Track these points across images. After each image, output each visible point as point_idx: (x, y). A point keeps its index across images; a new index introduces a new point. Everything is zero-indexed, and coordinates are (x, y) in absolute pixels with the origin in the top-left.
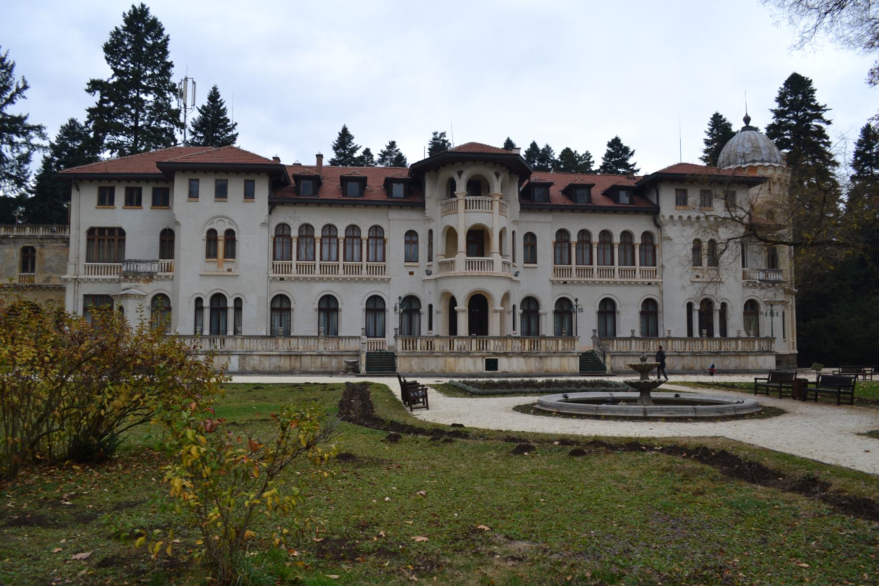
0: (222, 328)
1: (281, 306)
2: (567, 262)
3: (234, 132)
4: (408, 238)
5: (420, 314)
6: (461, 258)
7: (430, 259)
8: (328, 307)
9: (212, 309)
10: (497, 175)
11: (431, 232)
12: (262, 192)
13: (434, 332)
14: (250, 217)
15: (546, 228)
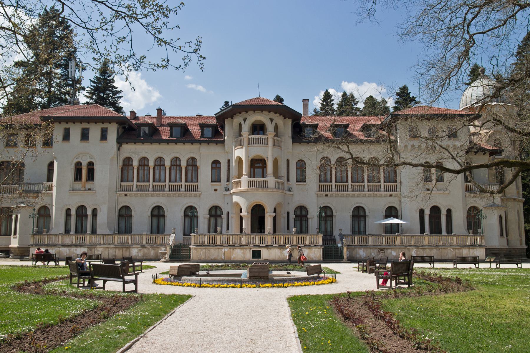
0: (362, 229)
3: (120, 95)
4: (214, 165)
6: (244, 179)
7: (228, 180)
9: (77, 215)
13: (230, 232)
14: (105, 153)
15: (312, 155)
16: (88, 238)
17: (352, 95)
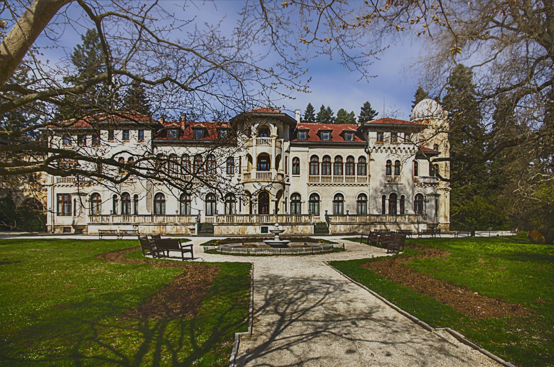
0: (316, 211)
15: (304, 155)
16: (132, 220)
17: (329, 109)
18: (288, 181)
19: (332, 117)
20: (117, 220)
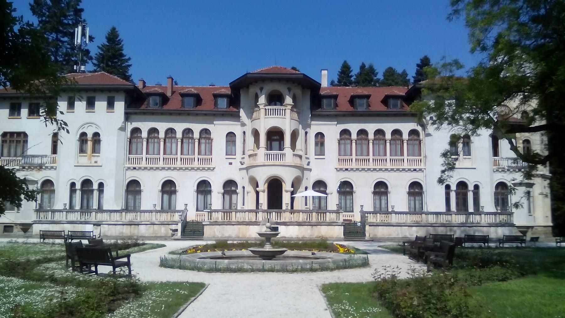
1: (133, 187)
2: (349, 154)
4: (229, 138)
5: (237, 194)
6: (262, 151)
8: (169, 187)
10: (289, 90)
11: (244, 133)
12: (120, 106)
15: (331, 130)
16: (93, 217)
18: (308, 164)
19: (375, 78)
20: (74, 217)
